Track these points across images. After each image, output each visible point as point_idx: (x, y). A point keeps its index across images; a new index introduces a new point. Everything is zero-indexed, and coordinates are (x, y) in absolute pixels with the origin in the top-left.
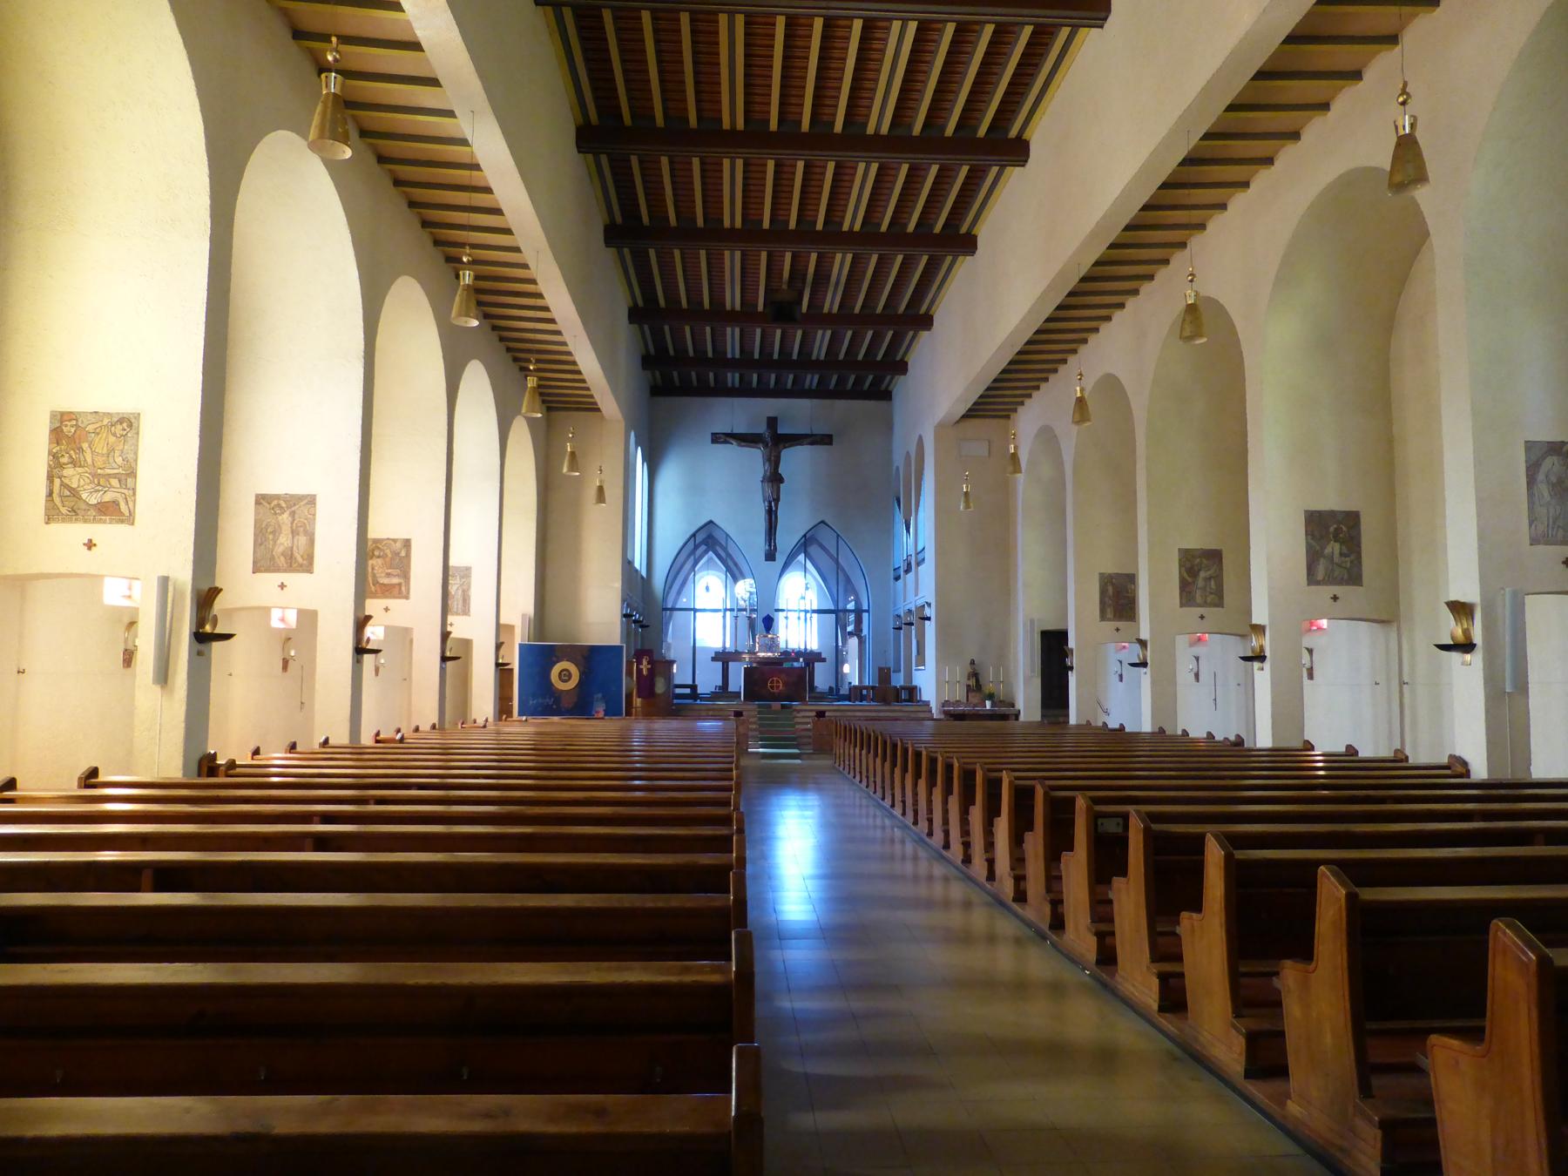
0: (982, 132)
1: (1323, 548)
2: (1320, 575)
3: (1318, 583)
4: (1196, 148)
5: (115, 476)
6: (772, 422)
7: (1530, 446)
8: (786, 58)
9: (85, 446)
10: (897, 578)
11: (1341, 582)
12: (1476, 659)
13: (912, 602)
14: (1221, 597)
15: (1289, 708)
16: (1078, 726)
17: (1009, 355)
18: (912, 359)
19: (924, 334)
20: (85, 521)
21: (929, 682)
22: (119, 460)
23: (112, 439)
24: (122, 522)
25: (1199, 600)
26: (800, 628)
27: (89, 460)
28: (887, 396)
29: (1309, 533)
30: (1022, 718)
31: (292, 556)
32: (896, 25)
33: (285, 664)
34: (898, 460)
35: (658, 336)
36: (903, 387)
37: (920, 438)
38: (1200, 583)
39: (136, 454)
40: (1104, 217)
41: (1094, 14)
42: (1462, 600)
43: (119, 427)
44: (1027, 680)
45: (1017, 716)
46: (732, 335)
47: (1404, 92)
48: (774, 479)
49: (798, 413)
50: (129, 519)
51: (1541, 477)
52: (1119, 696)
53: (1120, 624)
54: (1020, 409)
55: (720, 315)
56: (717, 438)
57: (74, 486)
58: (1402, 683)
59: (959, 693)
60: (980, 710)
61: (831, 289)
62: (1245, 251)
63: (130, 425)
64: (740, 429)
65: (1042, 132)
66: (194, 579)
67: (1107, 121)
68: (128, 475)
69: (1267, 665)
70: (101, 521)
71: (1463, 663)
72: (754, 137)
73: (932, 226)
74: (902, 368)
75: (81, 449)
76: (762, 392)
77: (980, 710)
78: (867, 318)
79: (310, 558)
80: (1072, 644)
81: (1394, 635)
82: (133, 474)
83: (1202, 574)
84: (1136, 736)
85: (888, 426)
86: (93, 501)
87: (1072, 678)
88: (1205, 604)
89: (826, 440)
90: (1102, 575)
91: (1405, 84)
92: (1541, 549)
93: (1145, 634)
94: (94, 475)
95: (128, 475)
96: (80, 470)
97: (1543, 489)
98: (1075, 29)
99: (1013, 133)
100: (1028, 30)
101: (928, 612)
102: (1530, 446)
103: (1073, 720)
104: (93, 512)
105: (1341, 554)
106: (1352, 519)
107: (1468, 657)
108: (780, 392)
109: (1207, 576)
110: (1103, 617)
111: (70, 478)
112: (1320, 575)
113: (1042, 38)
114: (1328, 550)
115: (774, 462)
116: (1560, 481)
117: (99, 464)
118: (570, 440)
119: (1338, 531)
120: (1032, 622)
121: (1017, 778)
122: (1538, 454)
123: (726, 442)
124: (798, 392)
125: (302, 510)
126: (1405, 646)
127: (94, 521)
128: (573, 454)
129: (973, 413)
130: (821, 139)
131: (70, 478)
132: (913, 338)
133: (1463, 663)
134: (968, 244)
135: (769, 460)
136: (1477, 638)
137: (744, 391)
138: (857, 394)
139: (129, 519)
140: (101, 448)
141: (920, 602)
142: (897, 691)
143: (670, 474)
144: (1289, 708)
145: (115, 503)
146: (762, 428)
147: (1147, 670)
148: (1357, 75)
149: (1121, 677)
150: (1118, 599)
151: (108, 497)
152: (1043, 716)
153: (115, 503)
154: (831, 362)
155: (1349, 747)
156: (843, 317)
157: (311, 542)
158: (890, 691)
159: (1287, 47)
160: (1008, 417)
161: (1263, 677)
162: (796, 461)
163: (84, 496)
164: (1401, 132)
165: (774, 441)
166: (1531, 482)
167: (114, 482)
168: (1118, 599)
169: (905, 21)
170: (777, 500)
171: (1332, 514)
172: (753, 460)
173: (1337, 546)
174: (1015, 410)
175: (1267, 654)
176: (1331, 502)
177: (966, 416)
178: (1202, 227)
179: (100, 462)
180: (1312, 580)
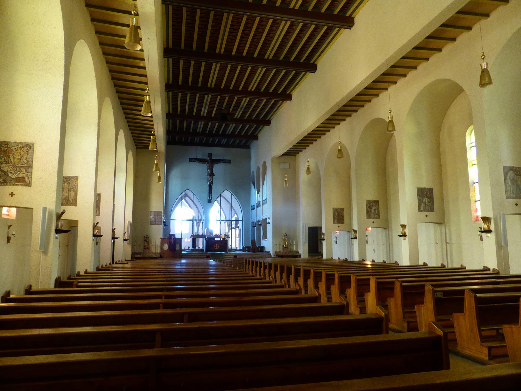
0: (292, 59)
1: (423, 199)
2: (422, 209)
3: (421, 211)
4: (387, 70)
5: (23, 167)
6: (210, 155)
7: (504, 168)
8: (270, 30)
9: (11, 155)
10: (252, 209)
11: (428, 211)
12: (492, 236)
13: (260, 218)
14: (379, 216)
15: (362, 251)
16: (326, 260)
17: (305, 134)
18: (260, 136)
19: (266, 127)
20: (10, 185)
21: (269, 244)
22: (25, 161)
23: (22, 153)
24: (26, 186)
25: (372, 217)
26: (216, 227)
27: (12, 161)
28: (249, 147)
29: (418, 195)
30: (302, 257)
31: (68, 200)
32: (284, 22)
33: (9, 240)
34: (253, 169)
35: (174, 124)
36: (254, 145)
37: (265, 162)
38: (373, 211)
39: (32, 159)
40: (351, 91)
41: (348, 25)
42: (487, 216)
43: (25, 148)
44: (304, 244)
45: (300, 256)
46: (201, 124)
47: (483, 55)
48: (212, 175)
49: (218, 152)
50: (29, 185)
51: (508, 178)
52: (337, 248)
53: (339, 225)
54: (300, 153)
55: (199, 117)
56: (191, 160)
57: (6, 171)
58: (447, 243)
59: (281, 249)
60: (288, 254)
61: (239, 110)
62: (398, 103)
63: (30, 148)
64: (199, 157)
65: (325, 62)
66: (56, 208)
67: (352, 59)
68: (29, 167)
69: (407, 238)
70: (17, 185)
71: (487, 237)
72: (227, 56)
73: (269, 90)
74: (256, 138)
75: (9, 157)
76: (207, 145)
77: (288, 254)
78: (249, 121)
79: (76, 200)
80: (324, 231)
81: (443, 228)
82: (31, 167)
83: (373, 208)
84: (352, 262)
85: (249, 158)
86: (14, 177)
87: (324, 243)
88: (374, 218)
89: (228, 162)
90: (333, 209)
91: (483, 53)
92: (509, 200)
93: (355, 227)
94: (15, 167)
95: (29, 167)
96: (9, 165)
97: (509, 182)
98: (340, 28)
99: (312, 62)
100: (325, 28)
101: (268, 221)
102: (504, 168)
103: (324, 257)
104: (13, 181)
105: (428, 202)
106: (431, 190)
107: (489, 235)
108: (213, 145)
109: (378, 210)
110: (334, 222)
111: (4, 167)
112: (422, 209)
113: (329, 31)
114: (424, 201)
115: (211, 169)
116: (513, 179)
117: (17, 162)
118: (156, 159)
119: (427, 194)
120: (306, 224)
121: (377, 279)
122: (508, 170)
123: (194, 161)
124: (219, 145)
125: (72, 182)
126: (447, 231)
127: (14, 185)
128: (157, 164)
129: (286, 154)
130: (249, 59)
131: (4, 167)
132: (262, 128)
133: (487, 237)
134: (289, 98)
135: (209, 168)
136: (492, 228)
137: (201, 144)
138: (239, 146)
139: (29, 185)
140: (17, 156)
141: (264, 218)
142: (257, 248)
143: (175, 173)
144: (362, 251)
145: (23, 178)
146: (206, 157)
147: (357, 240)
148: (440, 50)
149: (336, 242)
150: (339, 217)
151: (20, 175)
152: (309, 256)
153: (23, 178)
154: (233, 135)
155: (424, 263)
156: (241, 120)
157: (76, 195)
158: (254, 247)
159: (427, 40)
160: (296, 155)
161: (356, 243)
162: (218, 168)
163: (10, 175)
164: (483, 68)
165: (211, 162)
166: (505, 179)
167: (23, 170)
168: (339, 217)
169: (287, 21)
170: (212, 182)
171: (425, 189)
172: (203, 168)
173: (427, 199)
174: (298, 153)
175: (407, 234)
176: (425, 184)
177: (283, 155)
178: (378, 95)
179: (17, 161)
180: (420, 210)
